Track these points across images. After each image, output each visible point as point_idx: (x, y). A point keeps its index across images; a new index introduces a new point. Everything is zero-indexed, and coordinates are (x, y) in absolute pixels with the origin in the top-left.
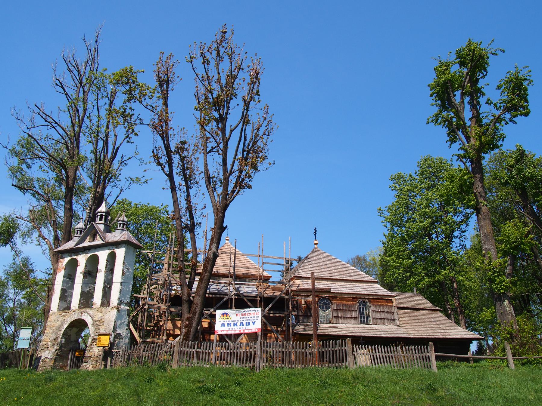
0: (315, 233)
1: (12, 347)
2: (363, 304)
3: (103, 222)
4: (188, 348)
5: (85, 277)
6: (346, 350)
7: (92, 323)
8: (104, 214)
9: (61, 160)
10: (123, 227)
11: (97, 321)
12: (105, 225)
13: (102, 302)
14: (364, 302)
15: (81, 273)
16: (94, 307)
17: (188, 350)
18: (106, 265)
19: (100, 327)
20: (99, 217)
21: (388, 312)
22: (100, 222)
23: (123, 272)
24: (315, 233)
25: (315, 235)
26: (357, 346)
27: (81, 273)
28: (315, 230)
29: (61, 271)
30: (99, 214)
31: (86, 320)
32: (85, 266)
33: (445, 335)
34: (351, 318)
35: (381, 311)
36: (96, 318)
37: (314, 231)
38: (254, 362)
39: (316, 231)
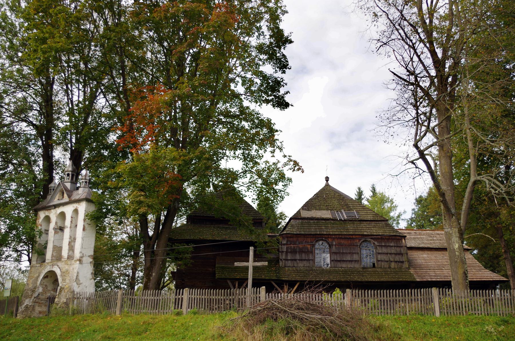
1: (3, 296)
3: (70, 180)
4: (233, 295)
6: (182, 298)
7: (60, 274)
8: (70, 173)
11: (64, 272)
16: (63, 260)
17: (179, 297)
19: (66, 278)
22: (67, 181)
31: (56, 272)
32: (315, 195)
36: (64, 270)
38: (181, 308)
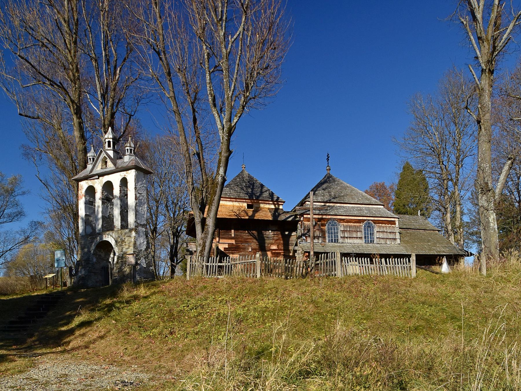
0: (328, 159)
2: (369, 226)
3: (111, 148)
5: (103, 203)
8: (111, 140)
9: (60, 83)
10: (131, 152)
12: (114, 150)
13: (121, 225)
14: (369, 223)
15: (100, 199)
16: (115, 229)
18: (120, 191)
20: (107, 143)
21: (390, 232)
23: (136, 197)
24: (328, 159)
25: (328, 161)
26: (346, 258)
27: (100, 199)
28: (327, 156)
29: (82, 198)
30: (107, 140)
33: (440, 252)
34: (357, 238)
35: (384, 232)
37: (327, 157)
39: (328, 157)
